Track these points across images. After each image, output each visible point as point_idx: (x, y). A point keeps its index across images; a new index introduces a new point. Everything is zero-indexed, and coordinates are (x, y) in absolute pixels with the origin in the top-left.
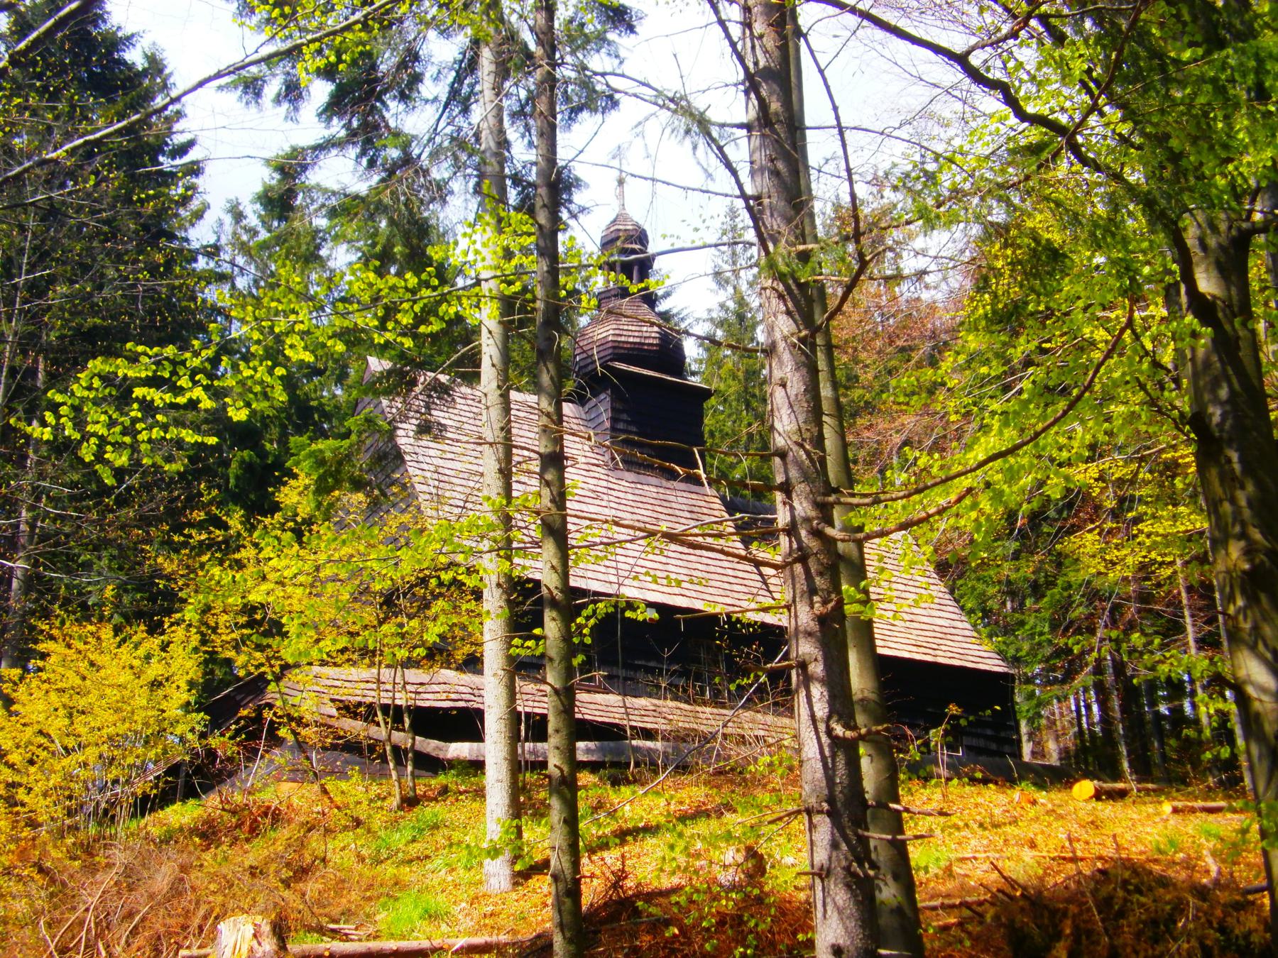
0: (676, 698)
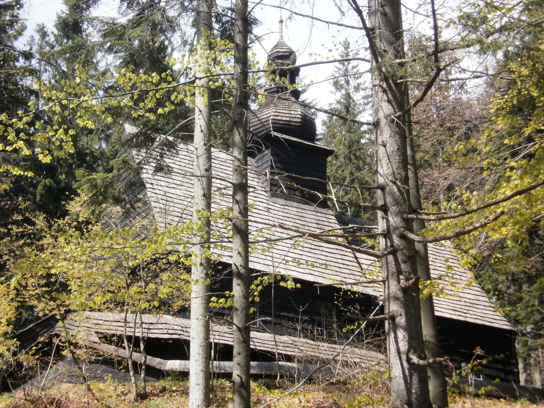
0: (306, 337)
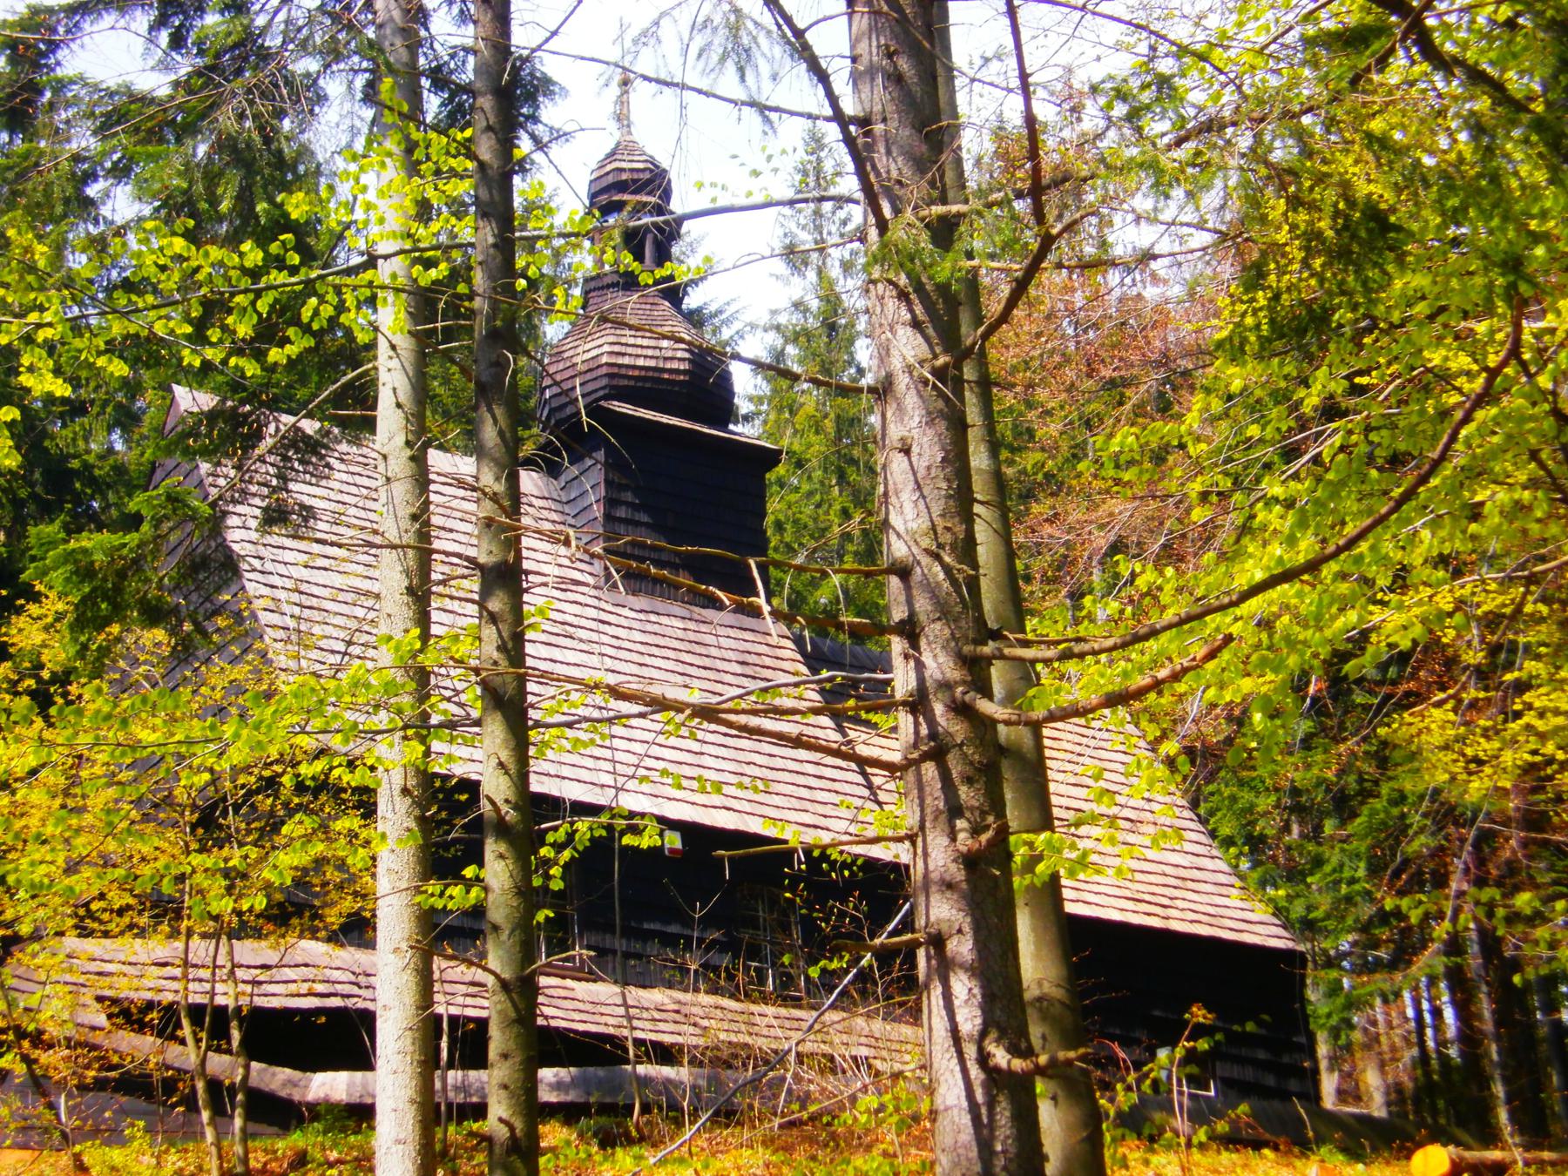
0: (714, 990)
